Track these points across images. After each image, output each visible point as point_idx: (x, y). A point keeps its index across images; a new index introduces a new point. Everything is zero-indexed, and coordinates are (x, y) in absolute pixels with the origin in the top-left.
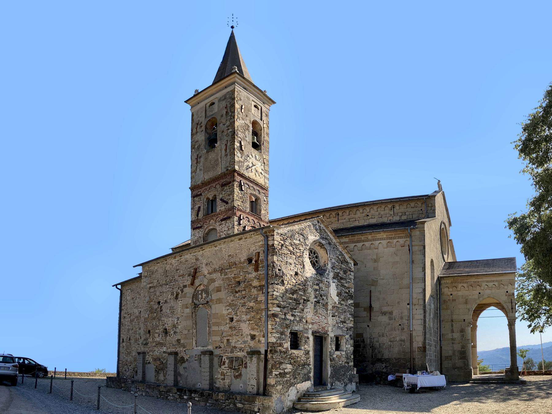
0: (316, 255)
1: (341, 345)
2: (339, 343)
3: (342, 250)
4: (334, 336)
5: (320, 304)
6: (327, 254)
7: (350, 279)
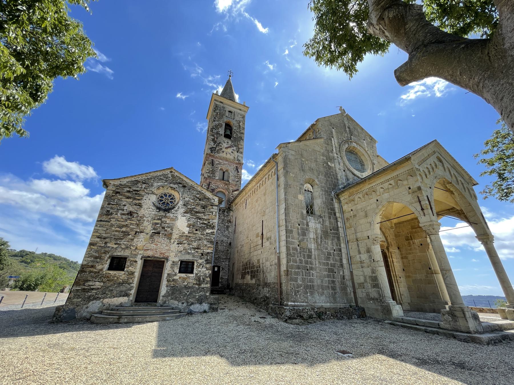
0: (168, 195)
5: (161, 234)
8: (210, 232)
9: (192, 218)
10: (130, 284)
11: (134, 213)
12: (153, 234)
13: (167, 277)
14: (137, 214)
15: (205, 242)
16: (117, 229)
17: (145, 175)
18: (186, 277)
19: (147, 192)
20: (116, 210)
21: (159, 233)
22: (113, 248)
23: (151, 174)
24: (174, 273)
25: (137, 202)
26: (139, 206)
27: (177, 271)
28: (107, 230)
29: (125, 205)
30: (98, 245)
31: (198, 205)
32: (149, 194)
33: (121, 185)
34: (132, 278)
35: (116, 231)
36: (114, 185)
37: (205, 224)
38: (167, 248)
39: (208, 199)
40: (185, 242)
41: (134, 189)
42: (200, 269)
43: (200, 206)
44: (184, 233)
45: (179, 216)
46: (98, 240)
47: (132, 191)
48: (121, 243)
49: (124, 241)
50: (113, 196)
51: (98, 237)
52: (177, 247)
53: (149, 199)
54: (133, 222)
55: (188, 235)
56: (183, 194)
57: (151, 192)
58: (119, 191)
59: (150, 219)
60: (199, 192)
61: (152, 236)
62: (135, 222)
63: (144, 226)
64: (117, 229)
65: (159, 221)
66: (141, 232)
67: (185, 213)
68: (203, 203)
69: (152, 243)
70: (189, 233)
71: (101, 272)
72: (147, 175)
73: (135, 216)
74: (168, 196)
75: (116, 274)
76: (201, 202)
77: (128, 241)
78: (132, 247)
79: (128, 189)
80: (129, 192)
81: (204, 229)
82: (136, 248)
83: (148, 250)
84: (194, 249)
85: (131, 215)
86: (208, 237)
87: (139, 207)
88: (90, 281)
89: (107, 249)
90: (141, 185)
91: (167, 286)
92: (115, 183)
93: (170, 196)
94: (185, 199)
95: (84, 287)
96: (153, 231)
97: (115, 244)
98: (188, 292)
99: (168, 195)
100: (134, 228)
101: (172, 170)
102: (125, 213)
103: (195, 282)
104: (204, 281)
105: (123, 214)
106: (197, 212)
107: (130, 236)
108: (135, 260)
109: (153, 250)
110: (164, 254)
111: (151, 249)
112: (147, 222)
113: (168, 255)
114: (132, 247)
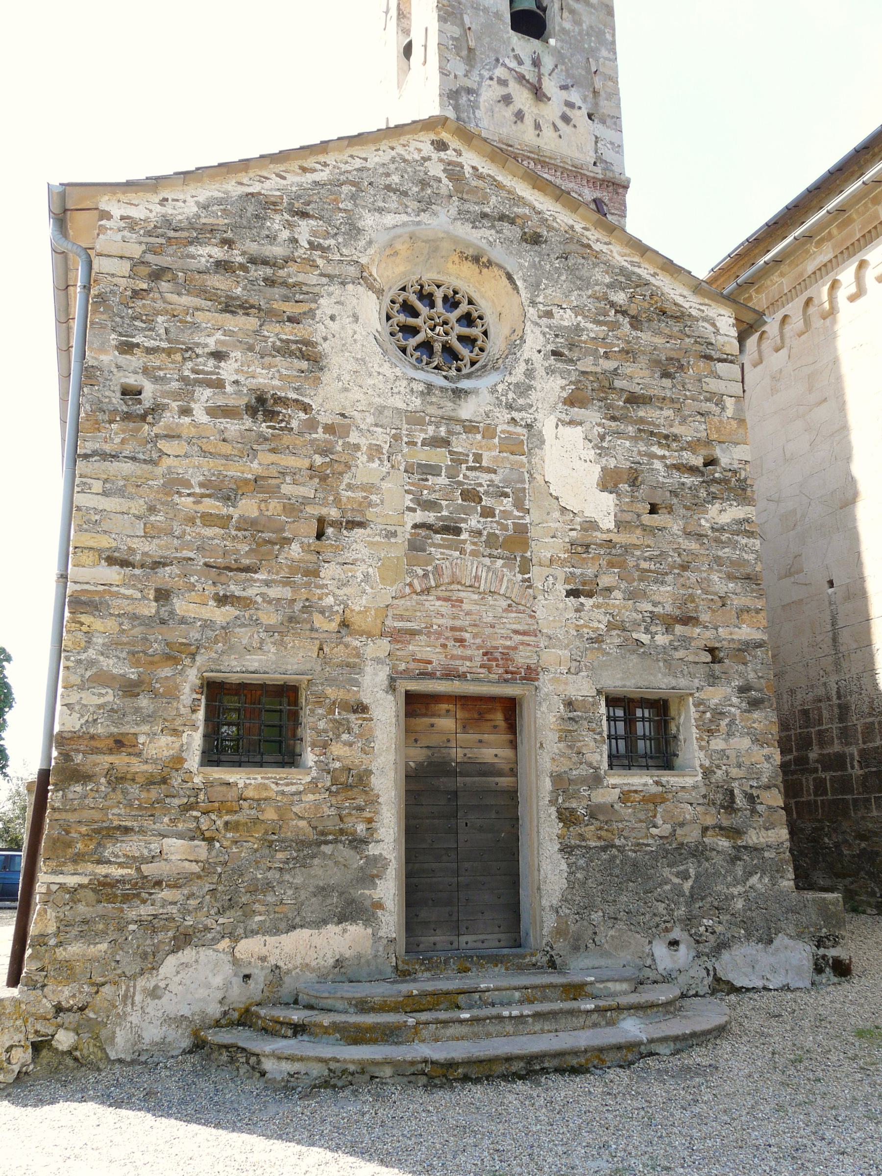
0: (464, 308)
1: (681, 737)
2: (674, 730)
3: (632, 263)
4: (599, 692)
5: (464, 536)
6: (516, 288)
7: (707, 400)
8: (725, 519)
9: (618, 434)
10: (358, 843)
11: (283, 401)
12: (423, 532)
13: (555, 791)
14: (306, 408)
15: (719, 584)
16: (212, 506)
17: (294, 165)
18: (655, 789)
19: (330, 270)
20: (175, 385)
21: (457, 531)
22: (207, 624)
23: (330, 159)
24: (584, 771)
25: (289, 332)
26: (304, 356)
27: (600, 757)
28: (152, 509)
29: (219, 356)
30: (118, 605)
31: (629, 353)
32: (343, 284)
33: (167, 222)
34: (360, 809)
35: (208, 519)
36: (131, 223)
37: (692, 470)
38: (512, 621)
39: (681, 317)
40: (605, 581)
41: (253, 248)
42: (717, 744)
43: (643, 360)
44: (591, 525)
45: (548, 426)
46: (113, 574)
47: (242, 267)
48: (251, 592)
49: (267, 583)
50: (136, 294)
51: (111, 561)
52: (572, 614)
53: (356, 318)
54: (290, 461)
55: (619, 538)
56: (535, 287)
57: (352, 271)
58: (164, 261)
59: (382, 438)
60: (622, 271)
61: (415, 546)
62: (306, 463)
63: (364, 488)
64: (212, 506)
65: (440, 457)
66: (353, 524)
67: (570, 401)
68: (659, 341)
69: (427, 591)
70: (619, 524)
71: (176, 781)
72: (310, 163)
73: (294, 424)
74: (458, 313)
75: (266, 787)
76: (645, 337)
77: (287, 582)
78: (318, 620)
79: (218, 253)
80: (223, 266)
81: (698, 506)
82: (344, 624)
83: (413, 633)
84: (669, 622)
85: (271, 415)
86: (725, 552)
87: (304, 365)
88: (127, 830)
89: (177, 635)
90: (289, 225)
91: (566, 850)
92: (137, 213)
93: (468, 320)
94: (549, 314)
95: (102, 870)
96: (420, 516)
97: (222, 600)
98: (685, 876)
99: (464, 308)
100: (306, 501)
101: (445, 136)
102: (231, 402)
103: (709, 821)
104: (753, 811)
105: (227, 412)
106: (634, 400)
107: (295, 550)
108: (351, 699)
109: (439, 634)
110: (506, 657)
111: (427, 631)
112: (371, 459)
113: (532, 661)
114: (318, 620)
